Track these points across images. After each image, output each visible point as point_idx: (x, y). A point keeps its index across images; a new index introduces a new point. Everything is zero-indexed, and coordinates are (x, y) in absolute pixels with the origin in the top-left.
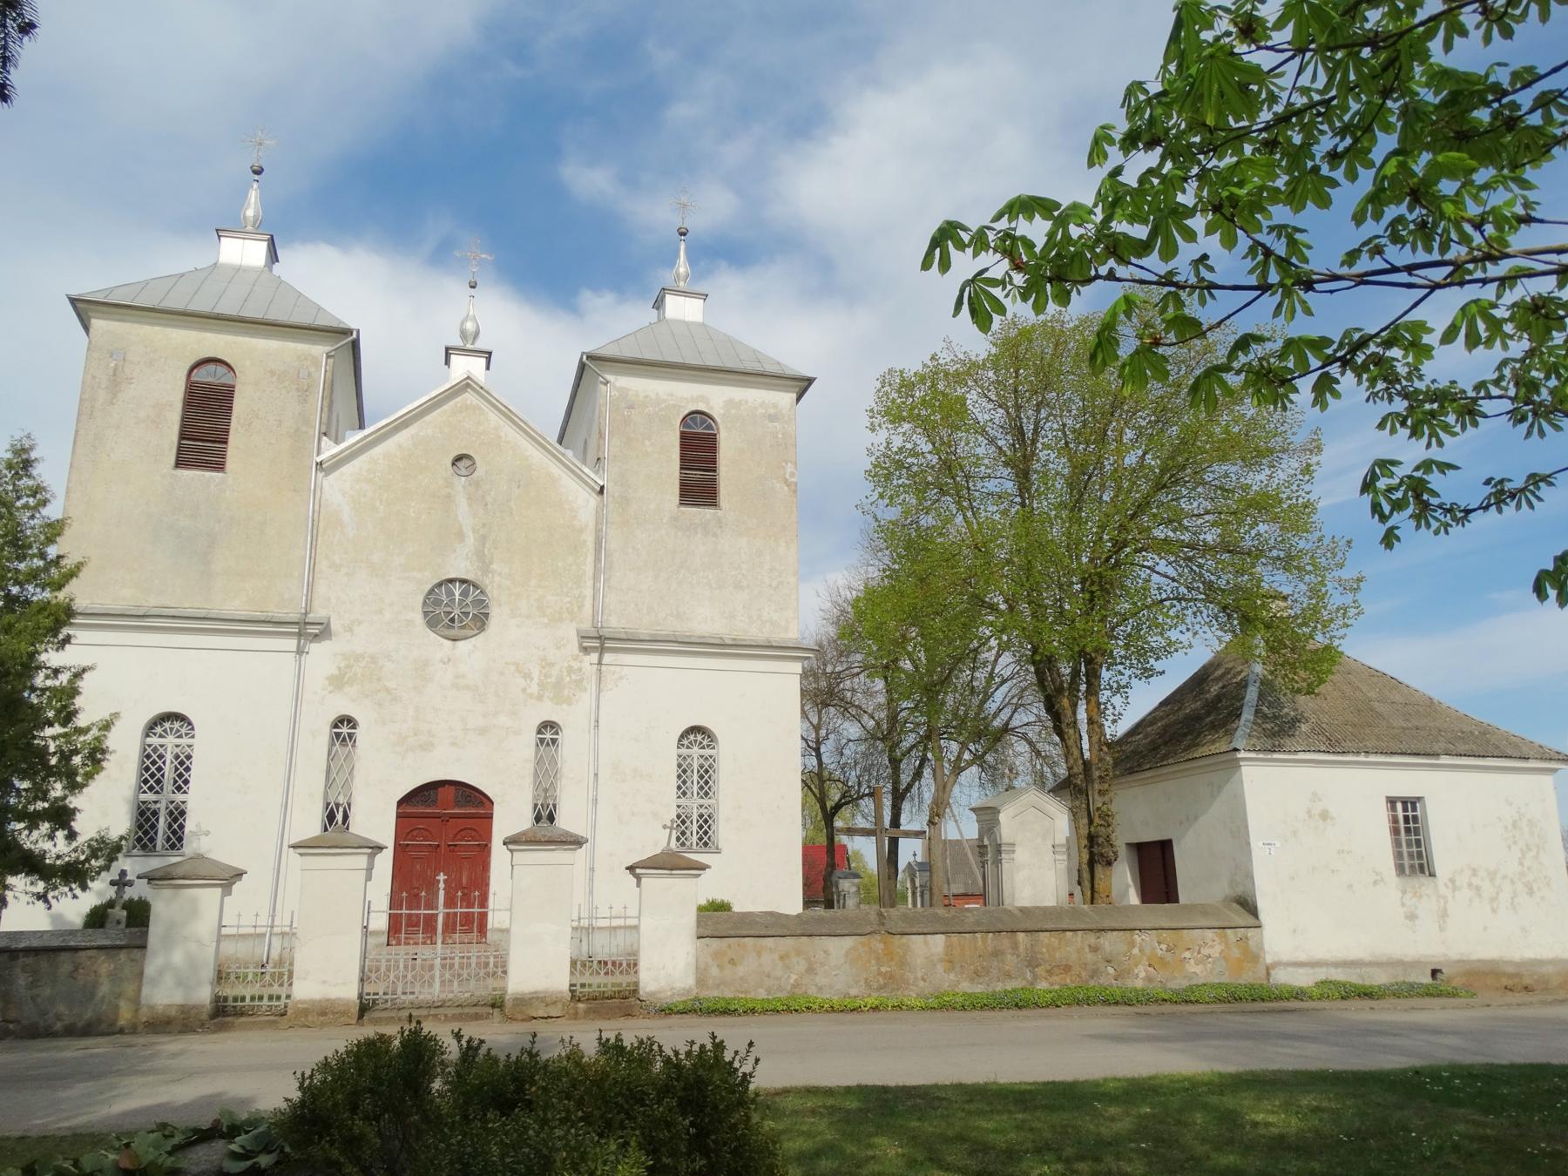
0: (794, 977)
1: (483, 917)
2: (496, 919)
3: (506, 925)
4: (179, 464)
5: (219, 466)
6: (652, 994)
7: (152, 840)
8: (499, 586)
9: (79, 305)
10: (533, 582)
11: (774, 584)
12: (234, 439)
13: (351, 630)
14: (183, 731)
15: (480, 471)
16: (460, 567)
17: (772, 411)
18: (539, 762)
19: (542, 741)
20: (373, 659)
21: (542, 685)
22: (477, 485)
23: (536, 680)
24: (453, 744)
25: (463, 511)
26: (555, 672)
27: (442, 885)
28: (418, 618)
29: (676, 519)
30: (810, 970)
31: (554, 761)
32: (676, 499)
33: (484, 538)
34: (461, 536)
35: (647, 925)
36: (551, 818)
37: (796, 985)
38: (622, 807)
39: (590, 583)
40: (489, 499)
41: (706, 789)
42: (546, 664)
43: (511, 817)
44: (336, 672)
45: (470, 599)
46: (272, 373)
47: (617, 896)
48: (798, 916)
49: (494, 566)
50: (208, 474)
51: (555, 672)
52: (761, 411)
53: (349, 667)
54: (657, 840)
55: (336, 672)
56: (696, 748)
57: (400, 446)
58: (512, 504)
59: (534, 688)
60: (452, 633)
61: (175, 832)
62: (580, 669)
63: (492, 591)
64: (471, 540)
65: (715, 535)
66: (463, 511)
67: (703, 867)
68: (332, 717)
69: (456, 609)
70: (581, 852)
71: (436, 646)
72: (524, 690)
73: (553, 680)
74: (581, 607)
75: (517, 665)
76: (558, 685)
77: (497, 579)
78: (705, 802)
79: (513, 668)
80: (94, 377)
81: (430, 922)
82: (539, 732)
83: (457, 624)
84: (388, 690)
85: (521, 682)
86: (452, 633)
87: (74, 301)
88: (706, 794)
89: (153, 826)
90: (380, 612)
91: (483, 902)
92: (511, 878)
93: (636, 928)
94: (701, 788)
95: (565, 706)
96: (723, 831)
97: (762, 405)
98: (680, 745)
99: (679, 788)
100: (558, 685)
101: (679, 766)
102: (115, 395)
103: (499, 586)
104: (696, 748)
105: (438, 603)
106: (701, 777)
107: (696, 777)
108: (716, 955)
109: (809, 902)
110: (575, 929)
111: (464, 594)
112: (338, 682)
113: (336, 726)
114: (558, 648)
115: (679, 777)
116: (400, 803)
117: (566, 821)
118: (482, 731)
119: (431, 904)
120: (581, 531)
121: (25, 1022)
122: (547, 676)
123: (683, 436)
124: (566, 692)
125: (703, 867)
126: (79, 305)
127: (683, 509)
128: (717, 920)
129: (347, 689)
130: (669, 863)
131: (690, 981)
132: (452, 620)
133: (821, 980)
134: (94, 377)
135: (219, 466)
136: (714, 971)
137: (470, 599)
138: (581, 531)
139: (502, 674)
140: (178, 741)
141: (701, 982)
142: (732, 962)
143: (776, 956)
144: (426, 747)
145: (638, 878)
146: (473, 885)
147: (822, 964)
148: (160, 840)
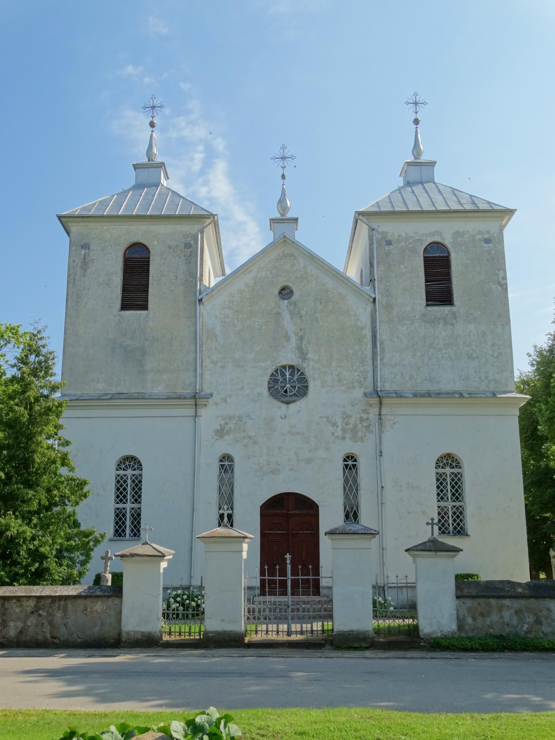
0: (526, 627)
1: (317, 583)
2: (324, 582)
3: (330, 585)
4: (124, 307)
5: (145, 307)
6: (428, 634)
7: (124, 531)
8: (313, 368)
9: (63, 220)
10: (334, 364)
11: (495, 354)
12: (152, 290)
13: (225, 401)
14: (454, 464)
15: (296, 296)
16: (288, 357)
17: (486, 236)
18: (346, 481)
19: (346, 466)
20: (240, 418)
21: (344, 430)
22: (295, 304)
23: (340, 427)
24: (291, 470)
25: (288, 324)
26: (352, 421)
27: (288, 561)
28: (266, 392)
29: (424, 315)
30: (538, 622)
31: (355, 481)
32: (424, 302)
33: (301, 338)
34: (287, 338)
35: (421, 589)
36: (356, 516)
37: (528, 632)
38: (403, 507)
39: (370, 362)
40: (303, 313)
41: (457, 495)
42: (346, 417)
43: (330, 517)
44: (219, 428)
45: (296, 377)
46: (170, 247)
47: (401, 568)
48: (527, 584)
49: (309, 355)
50: (138, 312)
51: (352, 421)
52: (478, 237)
53: (226, 424)
54: (425, 534)
55: (219, 428)
56: (448, 468)
57: (247, 285)
58: (318, 315)
59: (339, 432)
60: (286, 399)
61: (135, 527)
62: (368, 419)
63: (309, 373)
64: (294, 341)
65: (452, 324)
66: (288, 324)
67: (458, 550)
68: (219, 455)
69: (288, 385)
70: (375, 541)
71: (278, 409)
72: (333, 434)
73: (351, 426)
74: (365, 378)
75: (328, 418)
76: (354, 430)
77: (311, 363)
78: (457, 504)
79: (325, 420)
80: (74, 261)
81: (283, 584)
82: (345, 460)
83: (289, 394)
84: (250, 437)
85: (331, 429)
86: (286, 399)
87: (60, 217)
88: (457, 498)
89: (124, 523)
90: (242, 388)
91: (317, 572)
92: (331, 554)
93: (415, 587)
94: (453, 495)
95: (360, 443)
96: (471, 523)
97: (480, 232)
98: (119, 468)
99: (438, 495)
100: (354, 430)
101: (438, 480)
102: (85, 270)
103: (313, 368)
104: (448, 468)
105: (276, 381)
106: (453, 487)
107: (449, 487)
108: (469, 610)
109: (531, 579)
110: (374, 587)
111: (292, 374)
112: (221, 433)
113: (221, 461)
114: (353, 406)
115: (438, 487)
116: (262, 507)
117: (366, 519)
118: (309, 461)
119: (283, 573)
120: (362, 328)
121: (62, 639)
122: (347, 424)
123: (426, 259)
124: (360, 434)
125: (458, 550)
126: (63, 220)
127: (429, 308)
128: (467, 587)
129: (226, 437)
130: (433, 547)
131: (454, 627)
132: (286, 392)
133: (546, 629)
134: (74, 261)
135: (145, 307)
136: (470, 620)
137: (296, 377)
138: (362, 328)
139: (318, 424)
140: (134, 472)
141: (460, 627)
142: (482, 615)
143: (512, 611)
144: (275, 472)
145: (414, 556)
146: (310, 559)
147: (547, 618)
148: (128, 531)
